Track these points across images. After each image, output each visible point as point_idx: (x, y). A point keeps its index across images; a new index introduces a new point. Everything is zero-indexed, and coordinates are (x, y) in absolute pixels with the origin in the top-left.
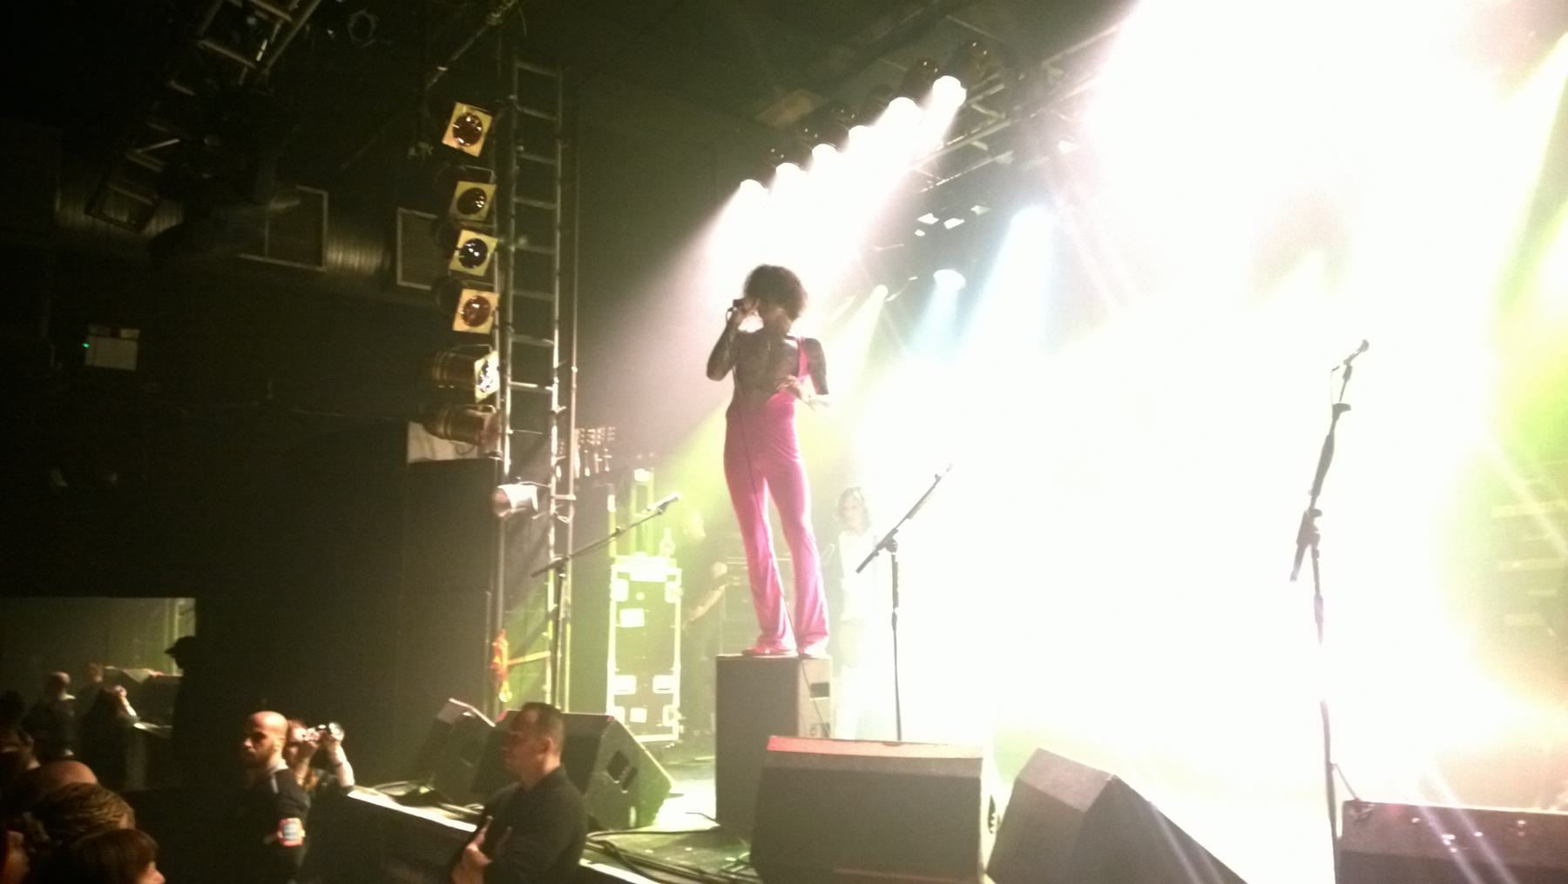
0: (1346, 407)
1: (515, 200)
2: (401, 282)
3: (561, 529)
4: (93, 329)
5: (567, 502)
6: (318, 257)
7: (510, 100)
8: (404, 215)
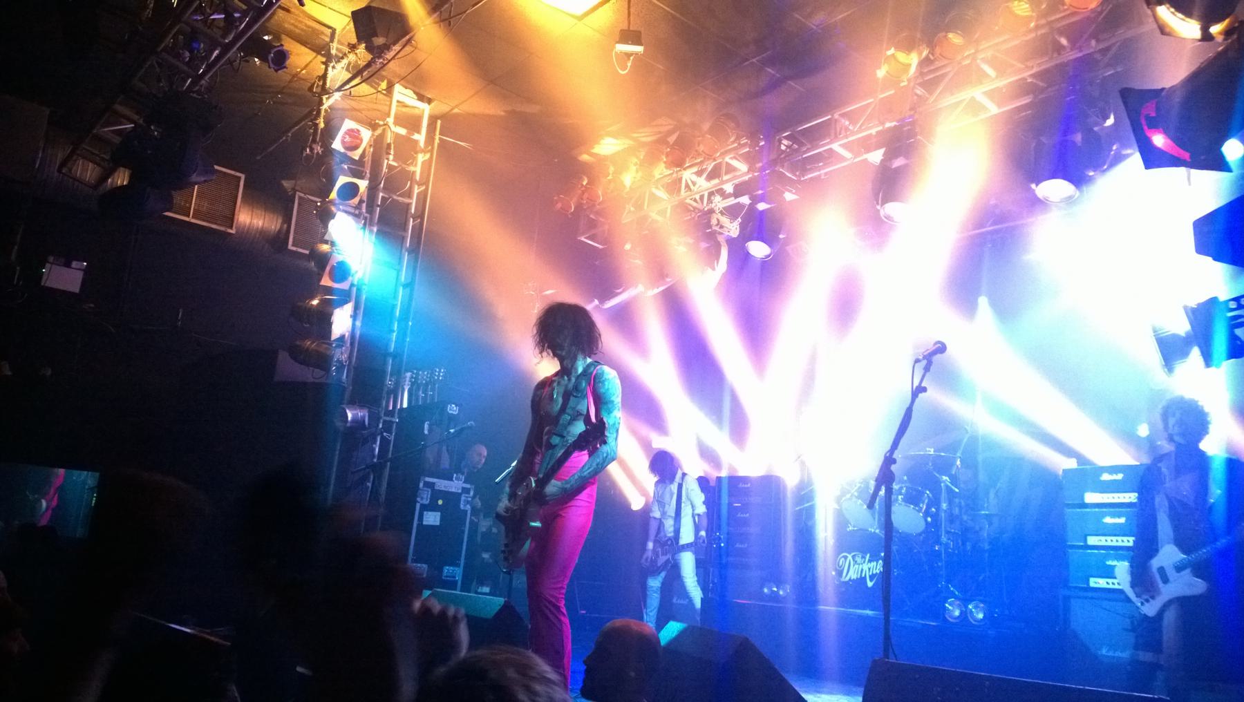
0: (924, 390)
2: (290, 247)
3: (385, 443)
4: (51, 259)
6: (230, 219)
7: (885, 78)
8: (300, 198)
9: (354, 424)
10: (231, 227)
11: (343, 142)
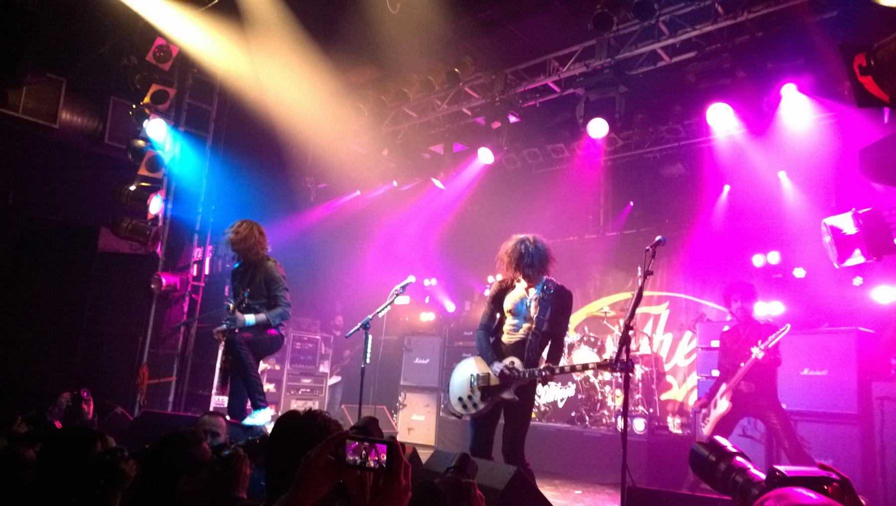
0: (652, 273)
1: (187, 100)
2: (106, 141)
3: (193, 303)
5: (198, 287)
6: (54, 117)
9: (168, 288)
10: (55, 123)
11: (154, 54)
